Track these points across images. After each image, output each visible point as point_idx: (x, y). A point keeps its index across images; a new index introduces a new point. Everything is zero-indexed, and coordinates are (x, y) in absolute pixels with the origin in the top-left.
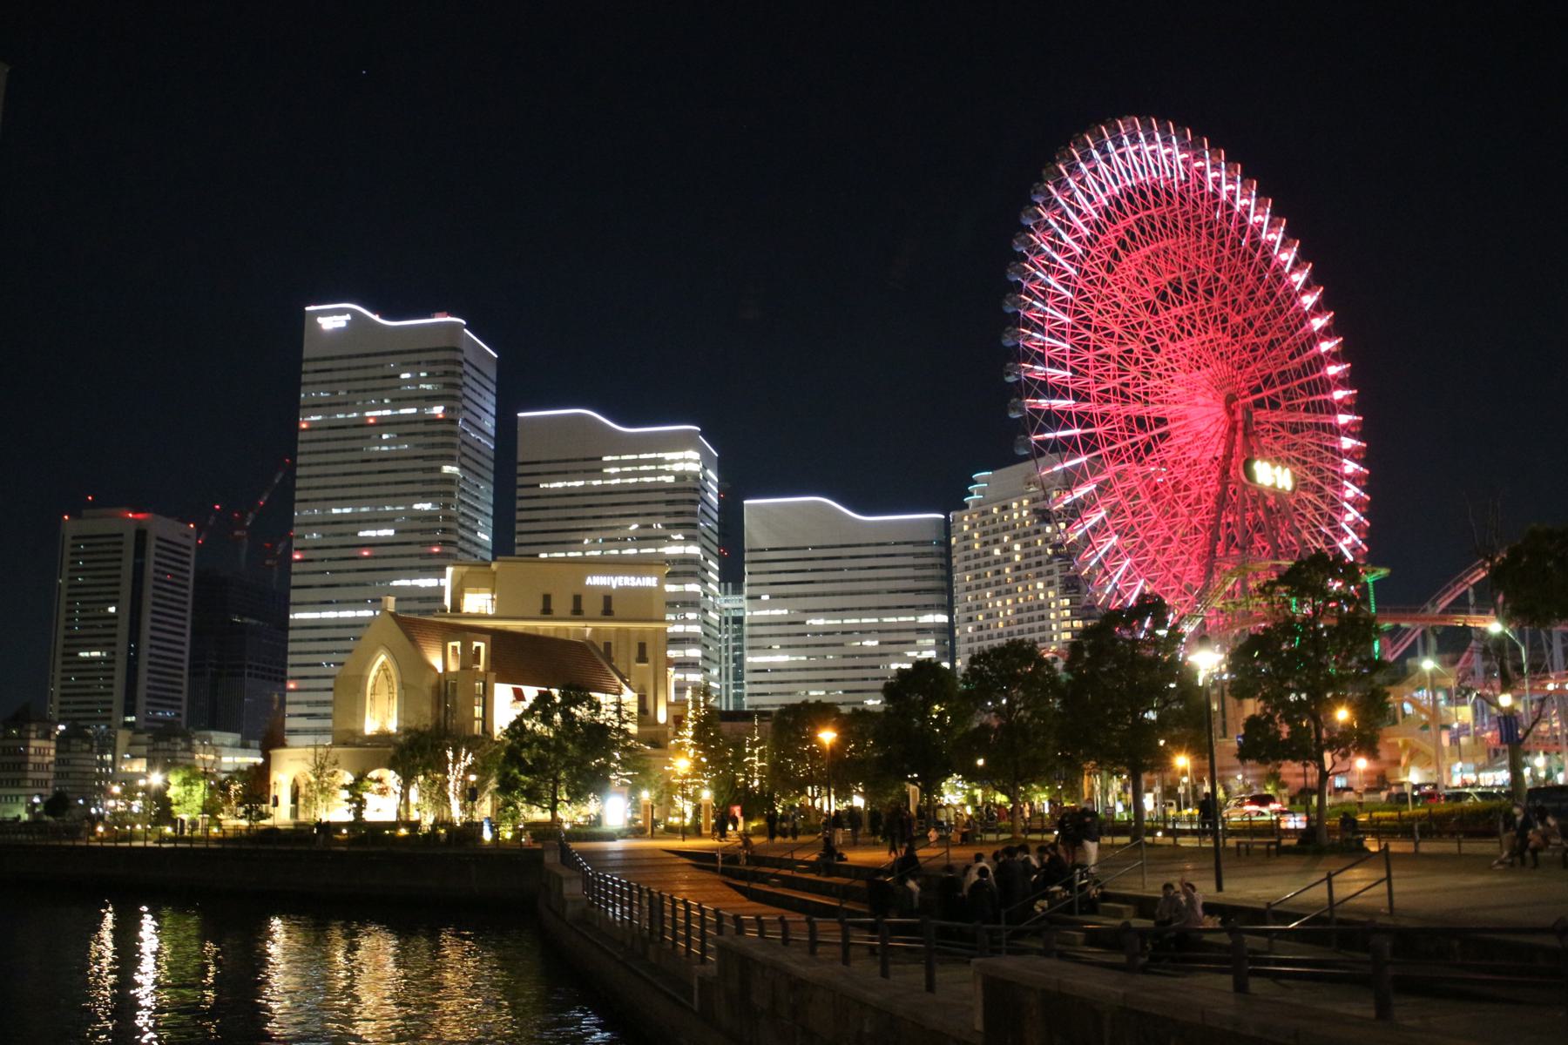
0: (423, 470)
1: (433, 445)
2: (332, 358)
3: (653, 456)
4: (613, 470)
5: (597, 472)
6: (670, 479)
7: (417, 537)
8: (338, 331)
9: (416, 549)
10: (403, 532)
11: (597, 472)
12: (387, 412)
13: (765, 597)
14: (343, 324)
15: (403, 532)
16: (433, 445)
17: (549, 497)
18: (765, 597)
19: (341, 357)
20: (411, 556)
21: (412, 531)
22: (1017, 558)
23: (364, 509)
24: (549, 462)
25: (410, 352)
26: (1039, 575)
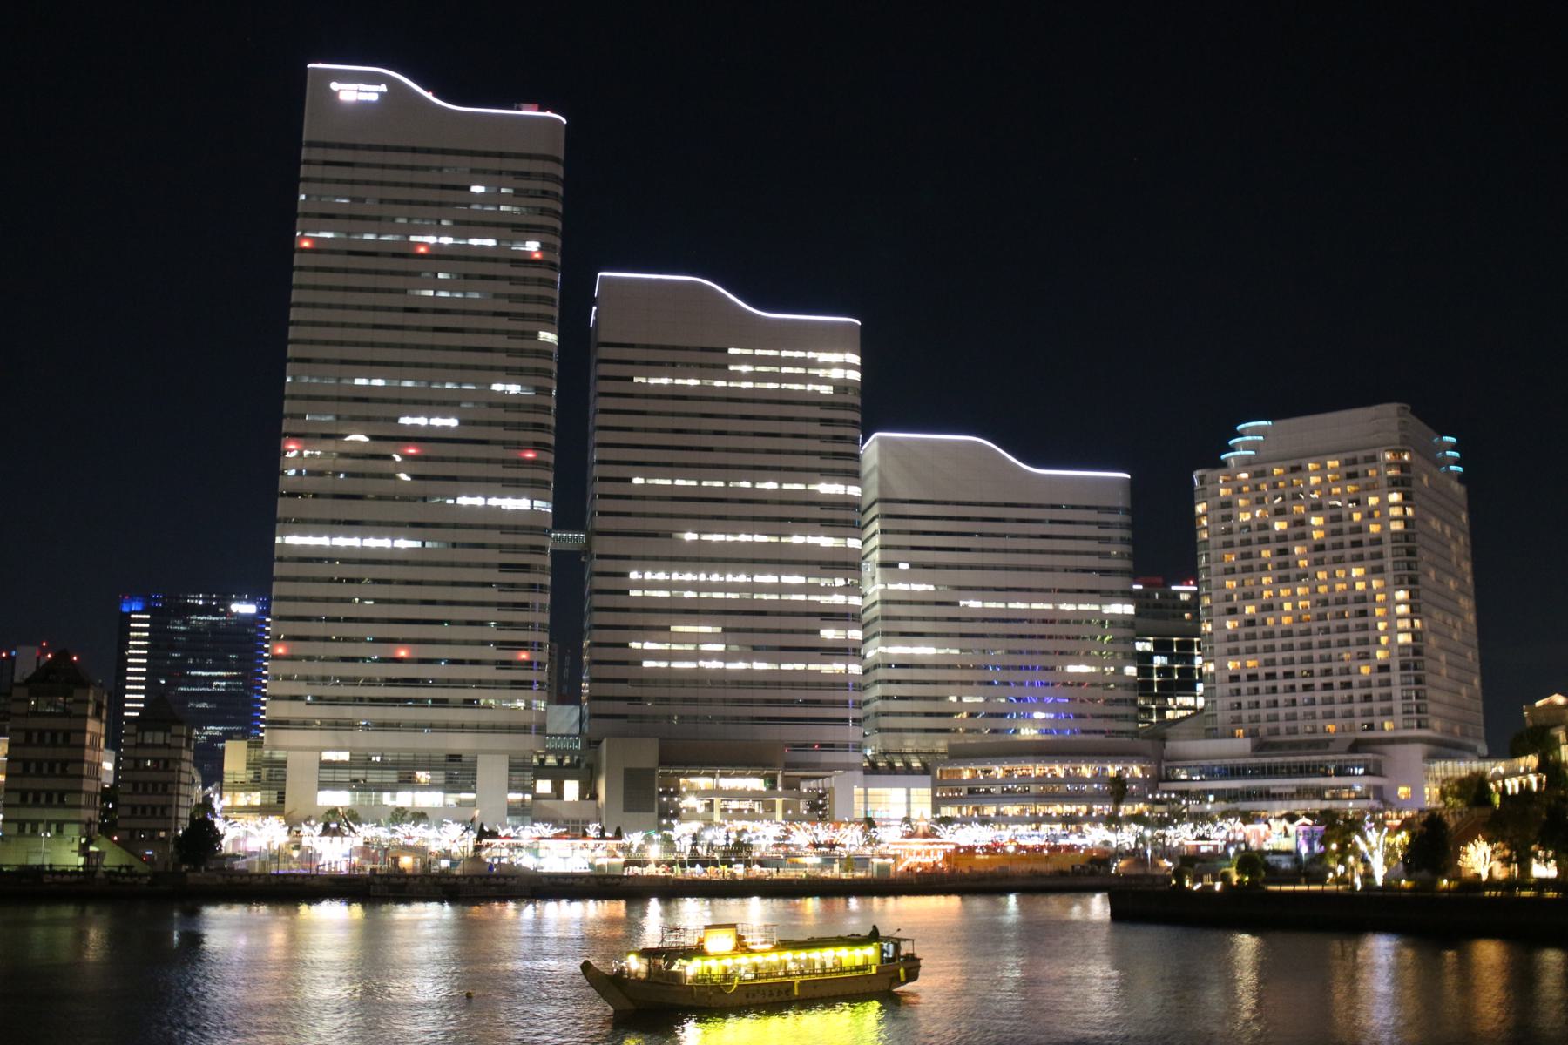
0: (509, 333)
1: (525, 299)
2: (354, 147)
3: (798, 354)
4: (745, 369)
5: (720, 369)
6: (826, 389)
9: (497, 452)
10: (474, 423)
11: (720, 369)
12: (447, 240)
13: (904, 566)
14: (374, 97)
15: (474, 423)
16: (525, 299)
17: (646, 396)
18: (904, 566)
19: (370, 148)
20: (488, 461)
22: (1317, 535)
23: (409, 384)
24: (648, 347)
25: (486, 154)
26: (1359, 559)
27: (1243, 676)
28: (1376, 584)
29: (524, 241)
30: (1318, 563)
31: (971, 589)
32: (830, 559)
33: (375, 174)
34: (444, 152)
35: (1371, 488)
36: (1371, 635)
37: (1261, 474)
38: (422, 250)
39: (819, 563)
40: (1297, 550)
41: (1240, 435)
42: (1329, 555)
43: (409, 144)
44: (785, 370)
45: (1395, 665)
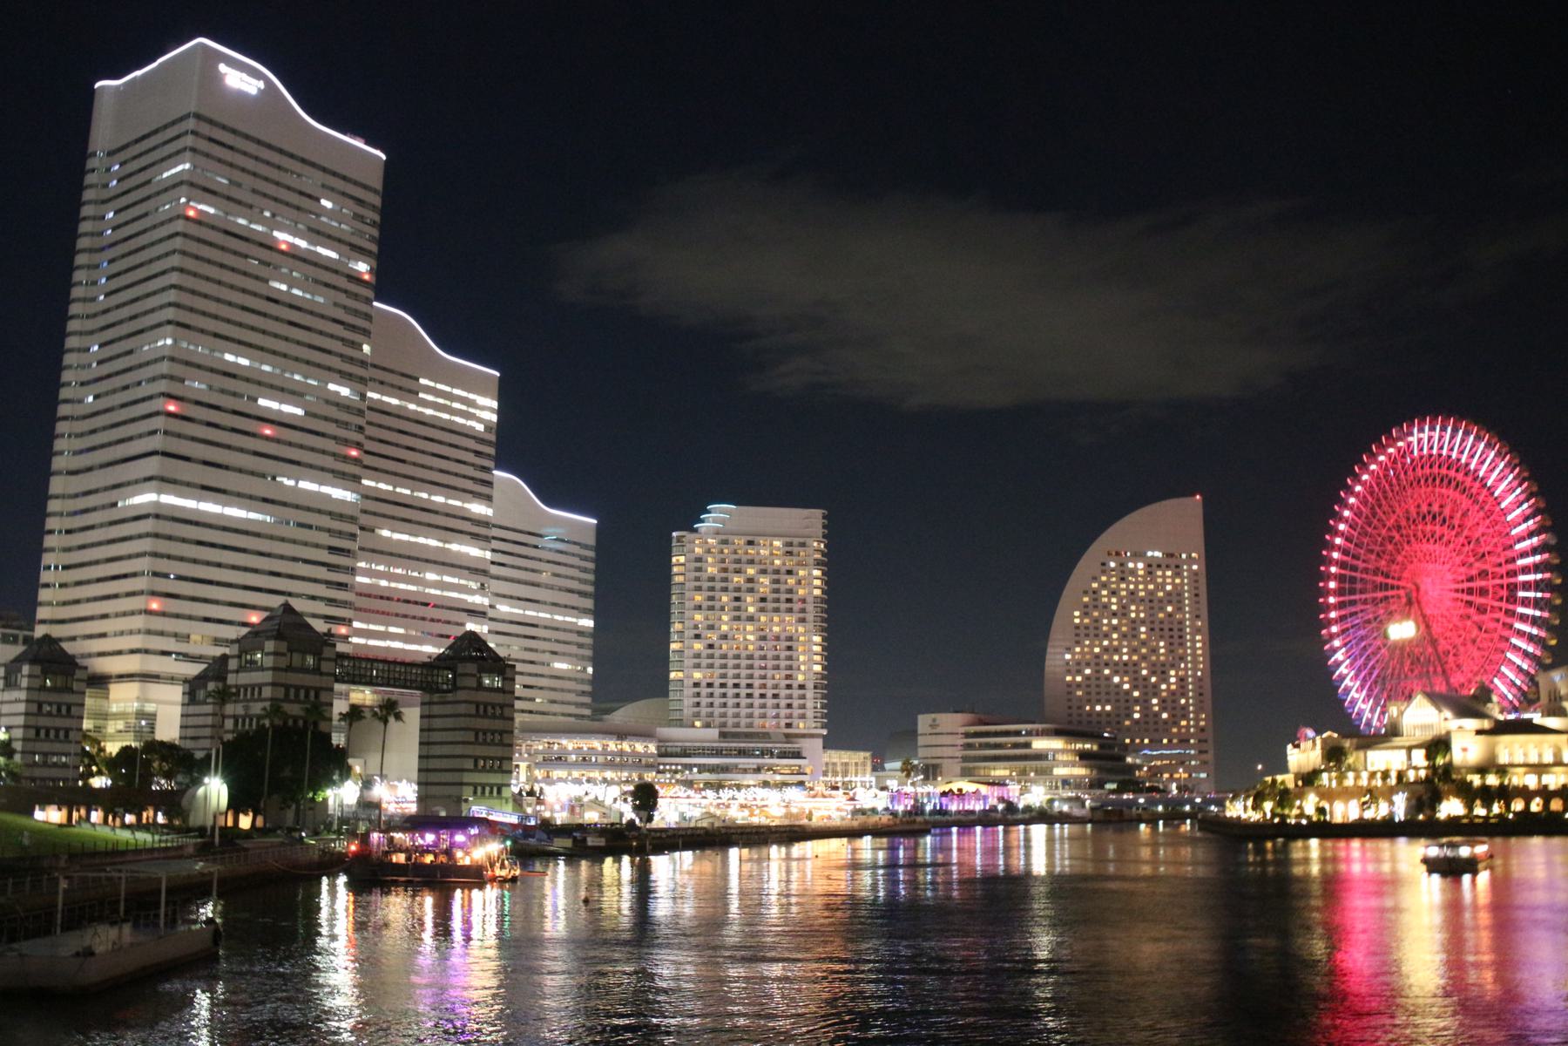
3: (448, 389)
4: (430, 398)
5: (412, 393)
6: (480, 427)
7: (331, 429)
8: (241, 95)
9: (330, 445)
10: (315, 416)
11: (412, 393)
12: (303, 244)
14: (253, 91)
15: (315, 416)
19: (247, 137)
21: (326, 419)
23: (266, 368)
27: (704, 684)
28: (801, 629)
29: (357, 260)
30: (762, 610)
31: (504, 596)
33: (250, 164)
34: (303, 161)
35: (801, 564)
36: (795, 664)
37: (725, 542)
38: (283, 247)
39: (468, 568)
40: (749, 599)
42: (770, 605)
43: (301, 154)
44: (472, 410)
45: (810, 685)
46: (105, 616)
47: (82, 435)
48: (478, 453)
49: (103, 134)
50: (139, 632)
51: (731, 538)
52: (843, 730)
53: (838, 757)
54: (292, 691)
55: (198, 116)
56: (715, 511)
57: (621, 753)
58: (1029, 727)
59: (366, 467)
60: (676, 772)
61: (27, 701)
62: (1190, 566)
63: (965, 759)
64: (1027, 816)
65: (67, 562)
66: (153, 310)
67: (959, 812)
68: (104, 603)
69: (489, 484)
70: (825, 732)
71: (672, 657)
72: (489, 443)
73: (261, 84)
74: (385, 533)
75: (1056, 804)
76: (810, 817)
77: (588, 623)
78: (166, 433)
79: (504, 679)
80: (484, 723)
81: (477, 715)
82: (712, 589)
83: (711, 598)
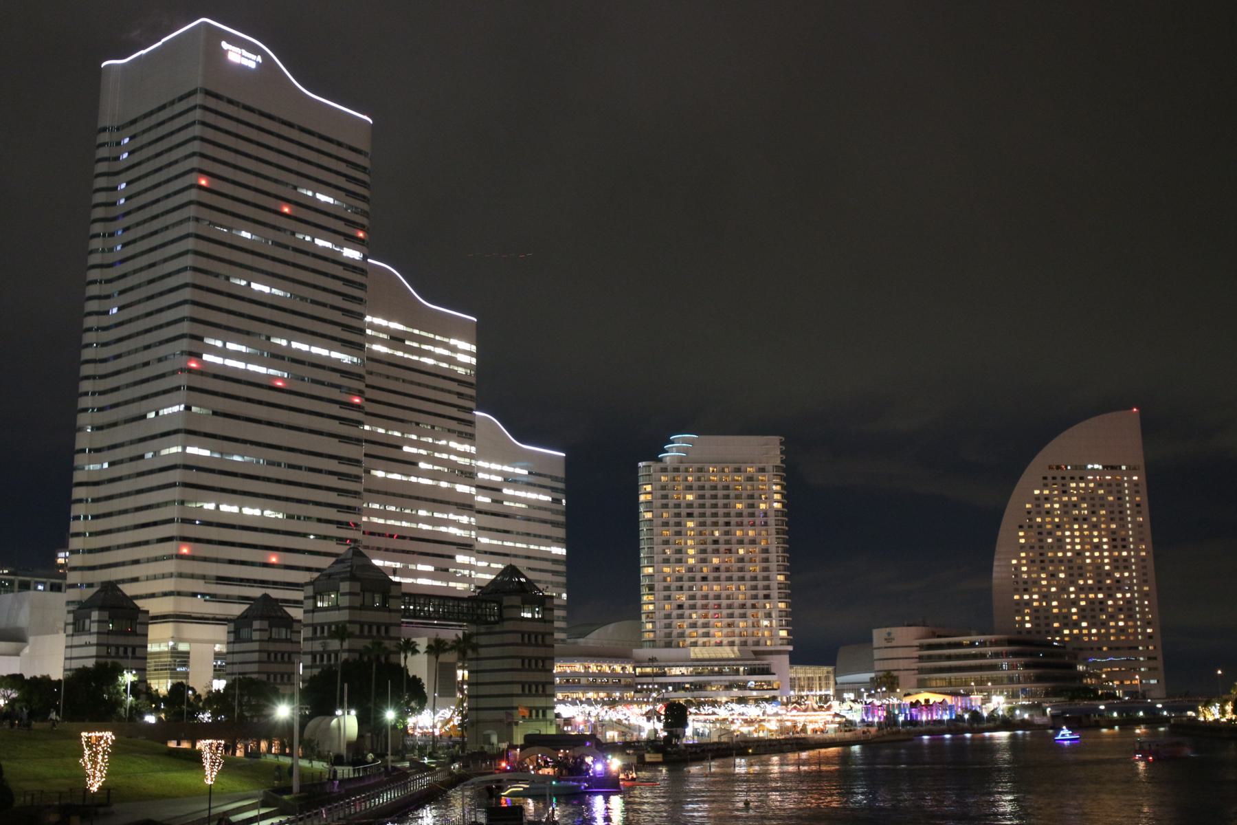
14: (253, 65)
32: (462, 501)
41: (672, 442)
44: (425, 347)
46: (136, 562)
47: (102, 393)
48: (460, 395)
49: (112, 108)
50: (171, 575)
51: (706, 466)
52: (811, 649)
53: (802, 672)
54: (366, 628)
55: (208, 93)
56: (678, 440)
57: (601, 674)
58: (982, 638)
59: (367, 414)
60: (651, 691)
61: (98, 645)
62: (1130, 477)
63: (921, 671)
64: (991, 725)
65: (95, 512)
66: (169, 275)
67: (928, 722)
68: (135, 549)
69: (470, 423)
70: (790, 648)
71: (645, 582)
72: (469, 385)
73: (259, 59)
74: (380, 474)
75: (1018, 712)
76: (804, 730)
77: (559, 551)
78: (190, 388)
79: (544, 609)
80: (529, 651)
81: (523, 644)
82: (728, 524)
83: (727, 533)
